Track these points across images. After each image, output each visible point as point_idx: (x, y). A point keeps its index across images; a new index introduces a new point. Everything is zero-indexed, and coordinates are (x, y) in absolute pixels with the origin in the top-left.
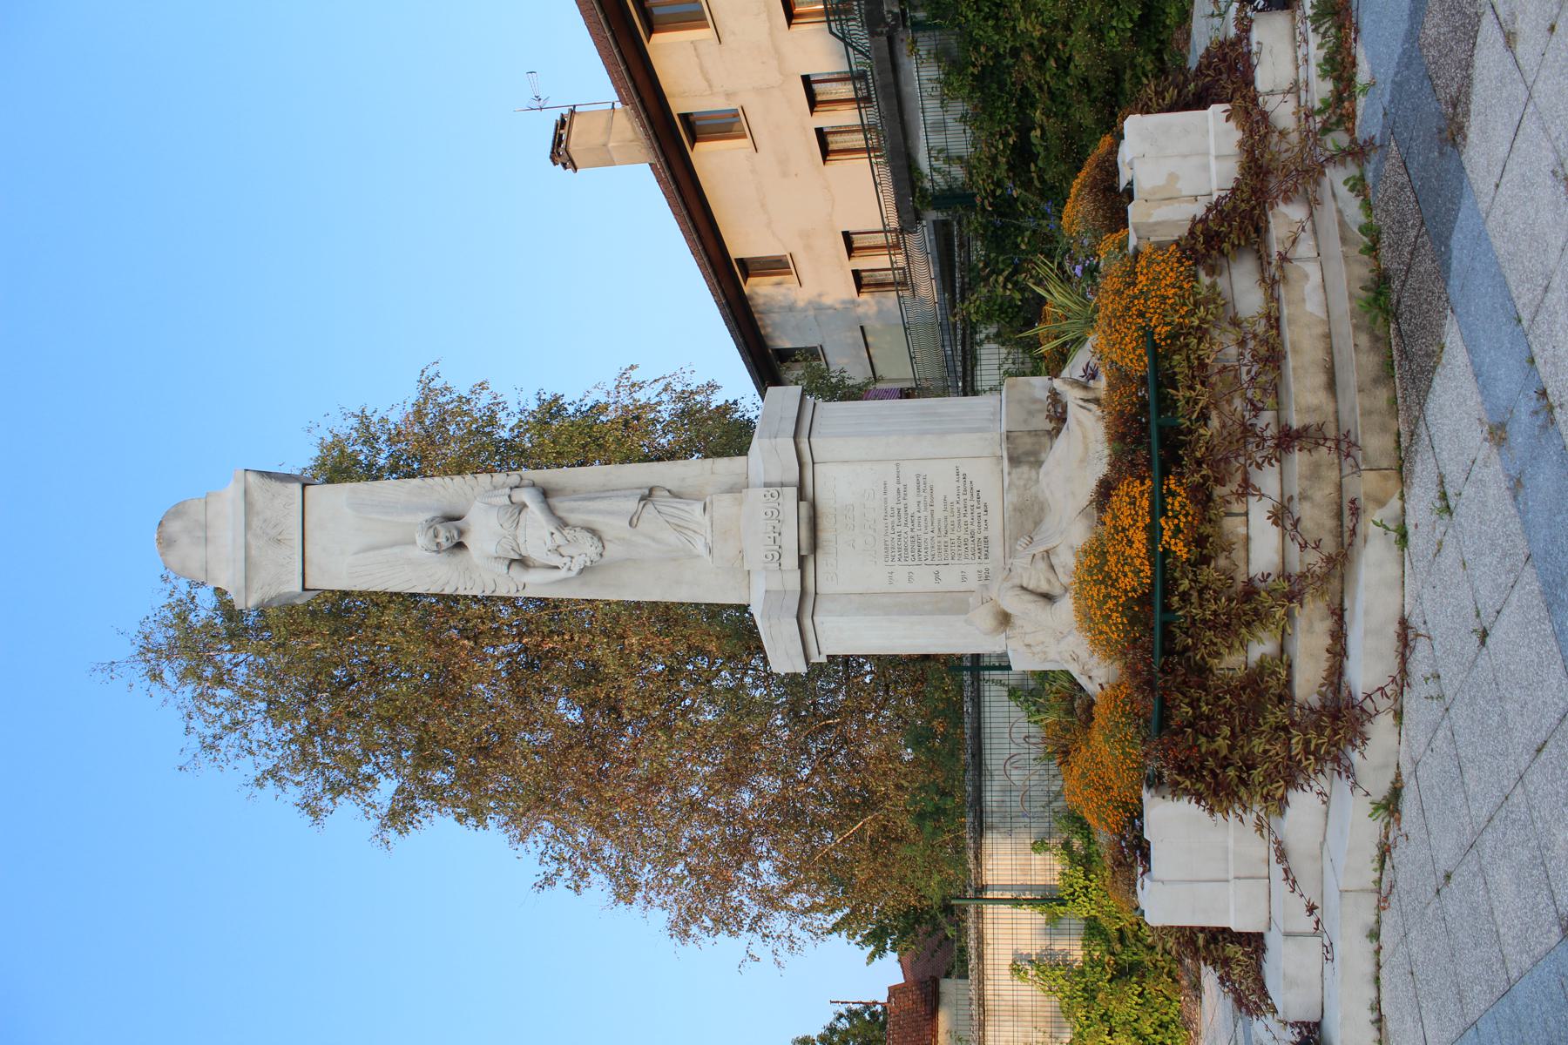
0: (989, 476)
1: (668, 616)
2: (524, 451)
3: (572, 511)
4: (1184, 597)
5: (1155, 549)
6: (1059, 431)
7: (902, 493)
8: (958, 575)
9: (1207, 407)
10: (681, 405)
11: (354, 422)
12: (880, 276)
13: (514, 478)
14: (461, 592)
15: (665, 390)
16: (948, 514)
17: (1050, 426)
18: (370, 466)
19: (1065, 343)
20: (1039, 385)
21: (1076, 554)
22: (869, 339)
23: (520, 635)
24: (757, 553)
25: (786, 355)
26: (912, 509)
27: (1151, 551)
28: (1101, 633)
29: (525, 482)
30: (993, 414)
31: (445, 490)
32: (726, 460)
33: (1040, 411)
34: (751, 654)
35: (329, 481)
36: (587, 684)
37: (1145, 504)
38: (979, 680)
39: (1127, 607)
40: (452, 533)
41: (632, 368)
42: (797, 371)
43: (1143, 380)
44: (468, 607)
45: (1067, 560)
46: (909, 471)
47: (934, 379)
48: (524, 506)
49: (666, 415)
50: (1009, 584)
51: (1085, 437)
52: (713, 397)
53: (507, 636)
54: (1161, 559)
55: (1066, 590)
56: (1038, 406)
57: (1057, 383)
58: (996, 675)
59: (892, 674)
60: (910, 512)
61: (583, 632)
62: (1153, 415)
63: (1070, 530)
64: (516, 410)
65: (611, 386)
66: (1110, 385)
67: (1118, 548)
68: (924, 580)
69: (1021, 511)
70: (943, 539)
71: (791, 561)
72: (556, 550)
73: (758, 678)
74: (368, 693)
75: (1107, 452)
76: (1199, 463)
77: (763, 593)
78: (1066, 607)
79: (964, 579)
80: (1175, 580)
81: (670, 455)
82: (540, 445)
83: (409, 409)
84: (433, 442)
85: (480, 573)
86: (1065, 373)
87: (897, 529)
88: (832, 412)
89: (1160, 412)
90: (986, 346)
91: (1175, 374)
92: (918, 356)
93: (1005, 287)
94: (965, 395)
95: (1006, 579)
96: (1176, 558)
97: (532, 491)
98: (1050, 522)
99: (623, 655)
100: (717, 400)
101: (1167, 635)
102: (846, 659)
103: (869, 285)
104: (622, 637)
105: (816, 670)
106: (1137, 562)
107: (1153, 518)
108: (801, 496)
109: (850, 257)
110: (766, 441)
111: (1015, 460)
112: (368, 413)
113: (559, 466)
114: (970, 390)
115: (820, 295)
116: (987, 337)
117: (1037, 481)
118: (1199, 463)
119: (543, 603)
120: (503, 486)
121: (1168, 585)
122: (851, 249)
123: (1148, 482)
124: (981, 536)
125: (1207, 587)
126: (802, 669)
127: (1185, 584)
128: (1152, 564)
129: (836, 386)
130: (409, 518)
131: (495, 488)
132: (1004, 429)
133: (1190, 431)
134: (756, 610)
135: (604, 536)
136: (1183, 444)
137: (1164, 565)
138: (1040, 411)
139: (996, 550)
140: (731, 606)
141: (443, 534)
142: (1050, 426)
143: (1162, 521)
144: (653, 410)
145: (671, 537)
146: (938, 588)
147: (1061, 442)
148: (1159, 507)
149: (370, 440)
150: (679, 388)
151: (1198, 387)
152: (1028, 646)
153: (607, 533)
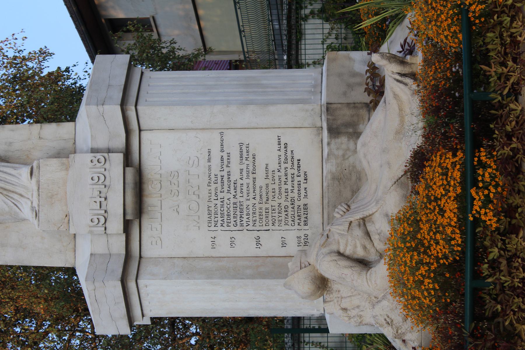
0: (308, 147)
4: (494, 265)
5: (466, 218)
9: (518, 83)
10: (12, 71)
16: (269, 181)
17: (367, 99)
19: (385, 20)
20: (358, 59)
21: (390, 221)
22: (201, 12)
24: (82, 219)
25: (119, 25)
27: (462, 221)
28: (414, 298)
30: (315, 86)
32: (54, 125)
33: (360, 84)
37: (457, 174)
38: (299, 342)
39: (438, 273)
42: (129, 41)
43: (458, 56)
45: (381, 227)
46: (233, 141)
47: (262, 52)
50: (325, 250)
51: (401, 110)
52: (45, 64)
54: (470, 227)
55: (381, 256)
56: (358, 80)
57: (375, 58)
58: (316, 337)
59: (218, 335)
60: (233, 179)
62: (466, 90)
63: (385, 200)
66: (425, 60)
67: (431, 216)
68: (245, 245)
70: (264, 206)
71: (116, 225)
73: (87, 339)
75: (421, 125)
76: (509, 136)
77: (87, 253)
78: (381, 272)
79: (284, 245)
80: (485, 248)
86: (384, 48)
87: (220, 195)
89: (473, 87)
90: (311, 21)
91: (488, 51)
92: (247, 29)
94: (290, 67)
95: (323, 245)
96: (486, 227)
98: (367, 191)
100: (50, 66)
101: (478, 301)
102: (173, 321)
105: (142, 333)
106: (449, 230)
107: (464, 189)
108: (127, 162)
110: (93, 108)
111: (334, 131)
114: (294, 62)
116: (312, 13)
117: (355, 151)
118: (509, 136)
121: (478, 254)
123: (460, 154)
124: (301, 203)
125: (515, 256)
127: (495, 253)
128: (463, 233)
132: (324, 100)
133: (501, 106)
134: (82, 275)
136: (494, 118)
137: (474, 234)
138: (360, 84)
139: (315, 216)
140: (59, 269)
142: (367, 99)
143: (473, 192)
147: (378, 115)
148: (470, 179)
150: (11, 54)
151: (510, 63)
152: (345, 310)
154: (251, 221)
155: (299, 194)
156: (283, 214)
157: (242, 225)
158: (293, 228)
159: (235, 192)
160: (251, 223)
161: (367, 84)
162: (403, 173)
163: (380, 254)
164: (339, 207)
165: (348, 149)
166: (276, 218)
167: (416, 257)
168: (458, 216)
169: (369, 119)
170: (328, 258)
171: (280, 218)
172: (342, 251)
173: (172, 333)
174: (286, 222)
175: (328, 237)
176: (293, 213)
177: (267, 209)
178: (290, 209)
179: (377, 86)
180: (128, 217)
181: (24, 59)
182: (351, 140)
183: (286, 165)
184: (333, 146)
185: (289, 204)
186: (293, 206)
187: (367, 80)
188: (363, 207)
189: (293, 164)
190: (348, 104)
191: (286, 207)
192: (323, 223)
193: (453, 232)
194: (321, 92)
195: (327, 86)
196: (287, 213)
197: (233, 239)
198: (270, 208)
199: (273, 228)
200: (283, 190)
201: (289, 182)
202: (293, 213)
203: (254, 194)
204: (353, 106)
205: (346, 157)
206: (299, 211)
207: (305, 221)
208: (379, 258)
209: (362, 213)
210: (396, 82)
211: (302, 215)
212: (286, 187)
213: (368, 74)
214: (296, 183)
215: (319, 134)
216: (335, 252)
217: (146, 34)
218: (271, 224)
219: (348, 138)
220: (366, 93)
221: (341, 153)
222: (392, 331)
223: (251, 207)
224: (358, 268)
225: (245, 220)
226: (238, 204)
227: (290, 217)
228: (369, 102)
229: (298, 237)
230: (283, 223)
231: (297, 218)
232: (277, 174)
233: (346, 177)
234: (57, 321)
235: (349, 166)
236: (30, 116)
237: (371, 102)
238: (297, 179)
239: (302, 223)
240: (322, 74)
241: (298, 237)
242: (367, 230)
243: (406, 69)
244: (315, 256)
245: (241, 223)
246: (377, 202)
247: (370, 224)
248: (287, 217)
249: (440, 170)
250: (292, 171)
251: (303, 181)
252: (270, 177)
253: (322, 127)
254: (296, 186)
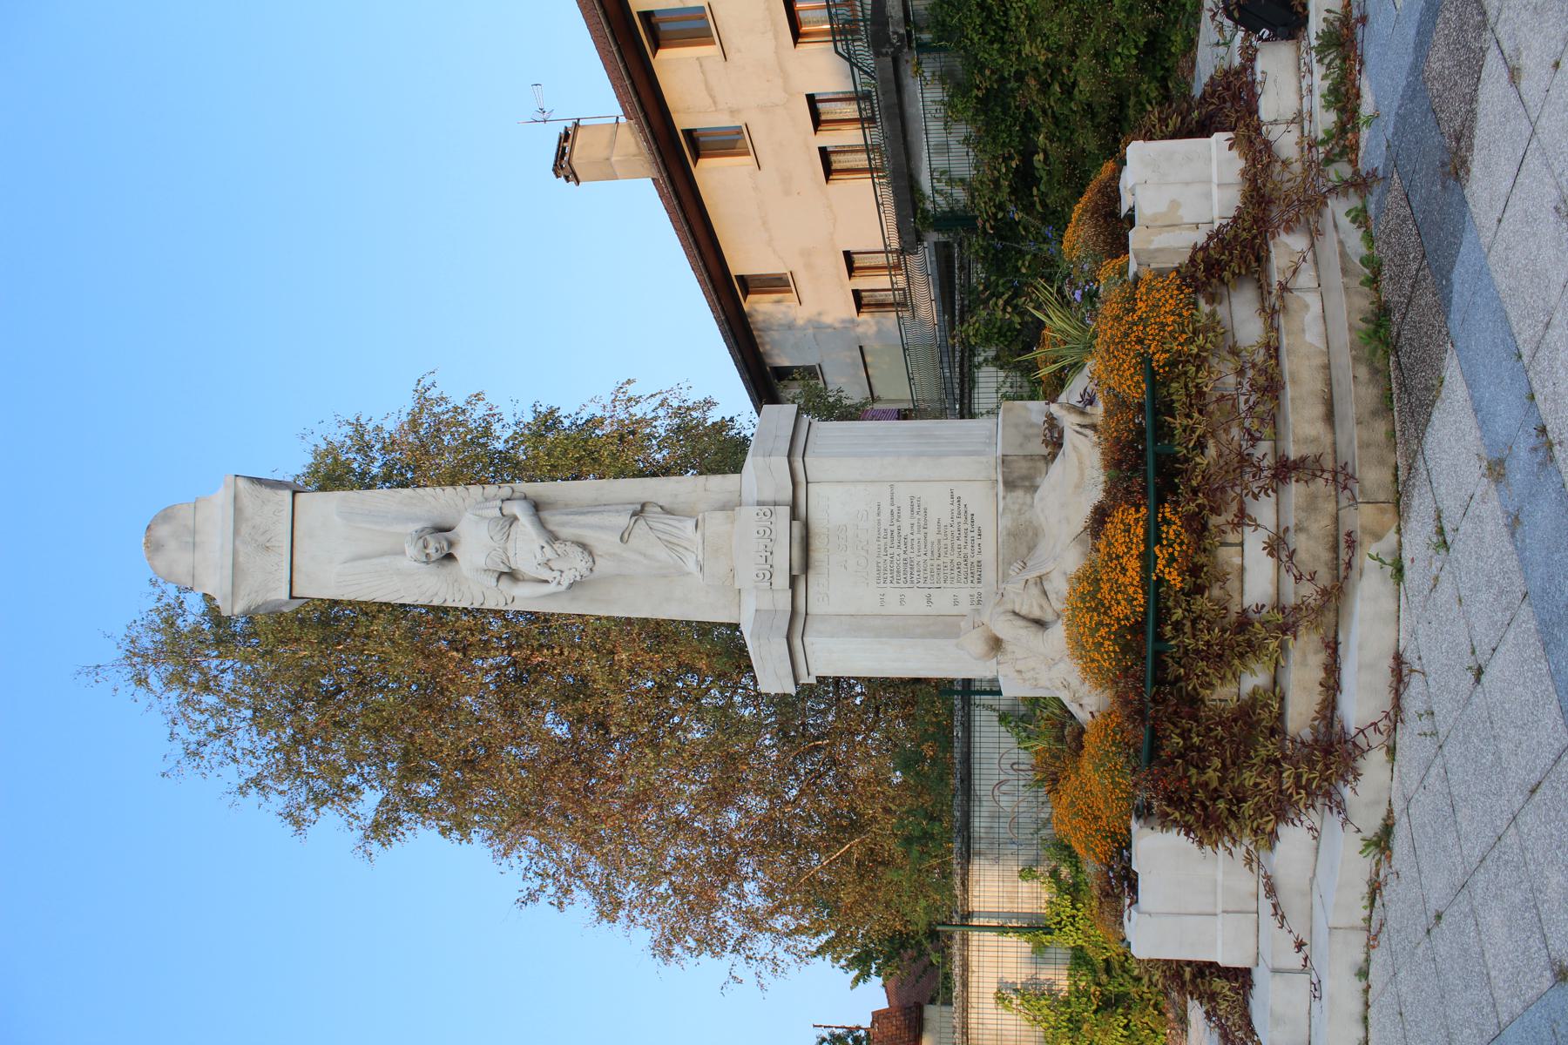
0: (983, 500)
1: (659, 632)
2: (518, 463)
3: (563, 525)
6: (1054, 456)
7: (895, 515)
8: (951, 598)
10: (677, 421)
11: (348, 430)
12: (880, 296)
13: (506, 490)
14: (449, 604)
15: (662, 405)
17: (1045, 451)
18: (364, 474)
23: (510, 648)
24: (747, 576)
25: (784, 373)
26: (906, 531)
29: (517, 495)
30: (990, 437)
31: (436, 501)
34: (741, 673)
35: (322, 488)
36: (576, 699)
40: (441, 544)
41: (629, 382)
42: (795, 389)
44: (458, 619)
46: (903, 493)
48: (515, 518)
49: (661, 431)
51: (1081, 463)
52: (709, 414)
53: (496, 649)
56: (1035, 431)
60: (903, 534)
61: (573, 646)
64: (512, 422)
65: (607, 400)
71: (782, 581)
72: (547, 564)
74: (355, 703)
77: (753, 610)
79: (956, 603)
81: (664, 471)
82: (535, 457)
83: (405, 418)
84: (427, 452)
85: (469, 586)
87: (890, 551)
88: (827, 432)
93: (1004, 310)
97: (523, 504)
99: (613, 672)
100: (714, 416)
103: (869, 305)
104: (612, 652)
105: (805, 691)
108: (794, 516)
111: (1010, 485)
112: (363, 421)
113: (554, 479)
115: (820, 314)
117: (1032, 506)
119: (533, 617)
120: (495, 498)
122: (851, 269)
124: (975, 560)
126: (792, 690)
129: (833, 406)
130: (399, 528)
131: (486, 500)
132: (999, 453)
135: (596, 551)
139: (989, 574)
140: (722, 624)
141: (432, 545)
142: (1045, 451)
144: (649, 424)
145: (662, 554)
146: (929, 611)
149: (364, 448)
153: (599, 548)
170: (1003, 618)
173: (836, 692)
180: (795, 573)
181: (688, 408)
204: (1030, 457)
217: (812, 382)
221: (1016, 507)
234: (721, 676)
236: (693, 467)
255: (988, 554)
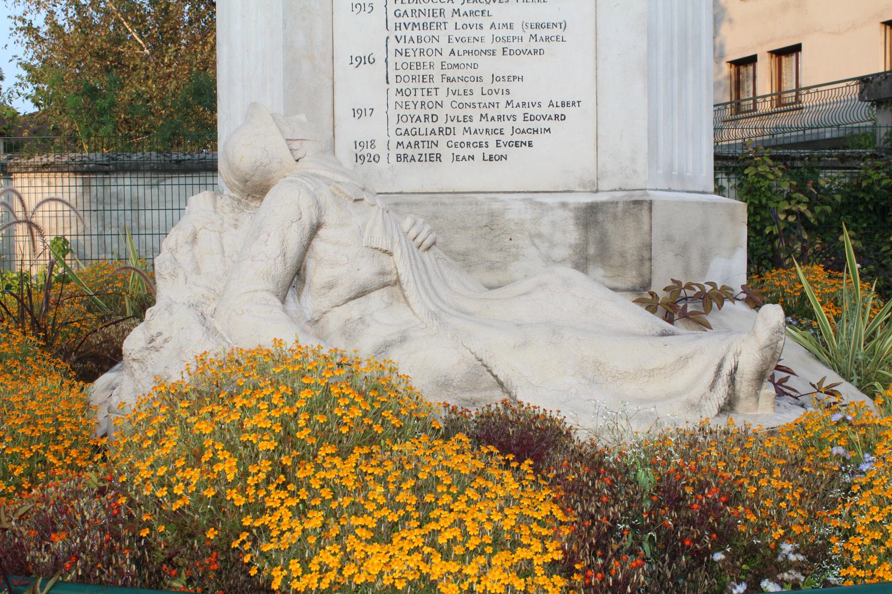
0: (561, 162)
6: (652, 307)
8: (365, 99)
12: (748, 86)
16: (487, 84)
17: (659, 287)
30: (681, 177)
33: (687, 270)
51: (651, 373)
56: (695, 265)
69: (490, 226)
70: (437, 72)
79: (358, 113)
93: (789, 212)
103: (738, 73)
109: (772, 52)
111: (590, 217)
115: (731, 21)
117: (550, 261)
122: (780, 54)
124: (442, 149)
132: (657, 196)
139: (415, 178)
142: (659, 287)
146: (342, 61)
154: (407, 46)
155: (461, 145)
156: (420, 112)
157: (397, 27)
158: (392, 132)
159: (465, 14)
160: (401, 46)
161: (689, 286)
162: (502, 379)
163: (317, 321)
164: (427, 227)
165: (552, 245)
166: (412, 98)
167: (263, 446)
168: (372, 585)
169: (615, 289)
170: (306, 202)
171: (412, 106)
172: (321, 232)
174: (404, 118)
175: (356, 200)
176: (423, 131)
177: (431, 78)
178: (430, 126)
179: (685, 307)
182: (571, 252)
183: (520, 118)
184: (560, 213)
185: (441, 123)
186: (437, 132)
187: (698, 285)
188: (426, 281)
189: (523, 132)
190: (649, 247)
191: (434, 118)
192: (401, 193)
193: (324, 569)
194: (669, 190)
195: (685, 203)
196: (422, 119)
197: (368, 9)
198: (432, 85)
199: (392, 92)
200: (468, 111)
201: (484, 124)
202: (423, 131)
203: (461, 53)
204: (645, 256)
205: (537, 241)
206: (426, 144)
207: (405, 156)
208: (309, 318)
209: (411, 278)
210: (717, 361)
211: (418, 149)
212: (476, 118)
213: (708, 288)
214: (484, 138)
215: (584, 186)
216: (320, 216)
218: (400, 86)
219: (577, 246)
220: (670, 284)
221: (545, 229)
222: (137, 348)
223: (434, 45)
224: (281, 270)
225: (409, 33)
226: (441, 20)
227: (414, 125)
228: (653, 289)
229: (373, 142)
230: (402, 112)
231: (413, 139)
232: (502, 99)
233: (496, 240)
235: (517, 247)
237: (652, 294)
238: (492, 139)
239: (401, 151)
240: (703, 193)
241: (373, 142)
242: (372, 291)
243: (745, 384)
244: (313, 171)
245: (403, 26)
246: (435, 316)
247: (386, 298)
248: (414, 120)
249: (508, 524)
250: (508, 131)
251: (488, 152)
252: (497, 85)
253: (597, 191)
254: (478, 138)
255: (450, 175)
